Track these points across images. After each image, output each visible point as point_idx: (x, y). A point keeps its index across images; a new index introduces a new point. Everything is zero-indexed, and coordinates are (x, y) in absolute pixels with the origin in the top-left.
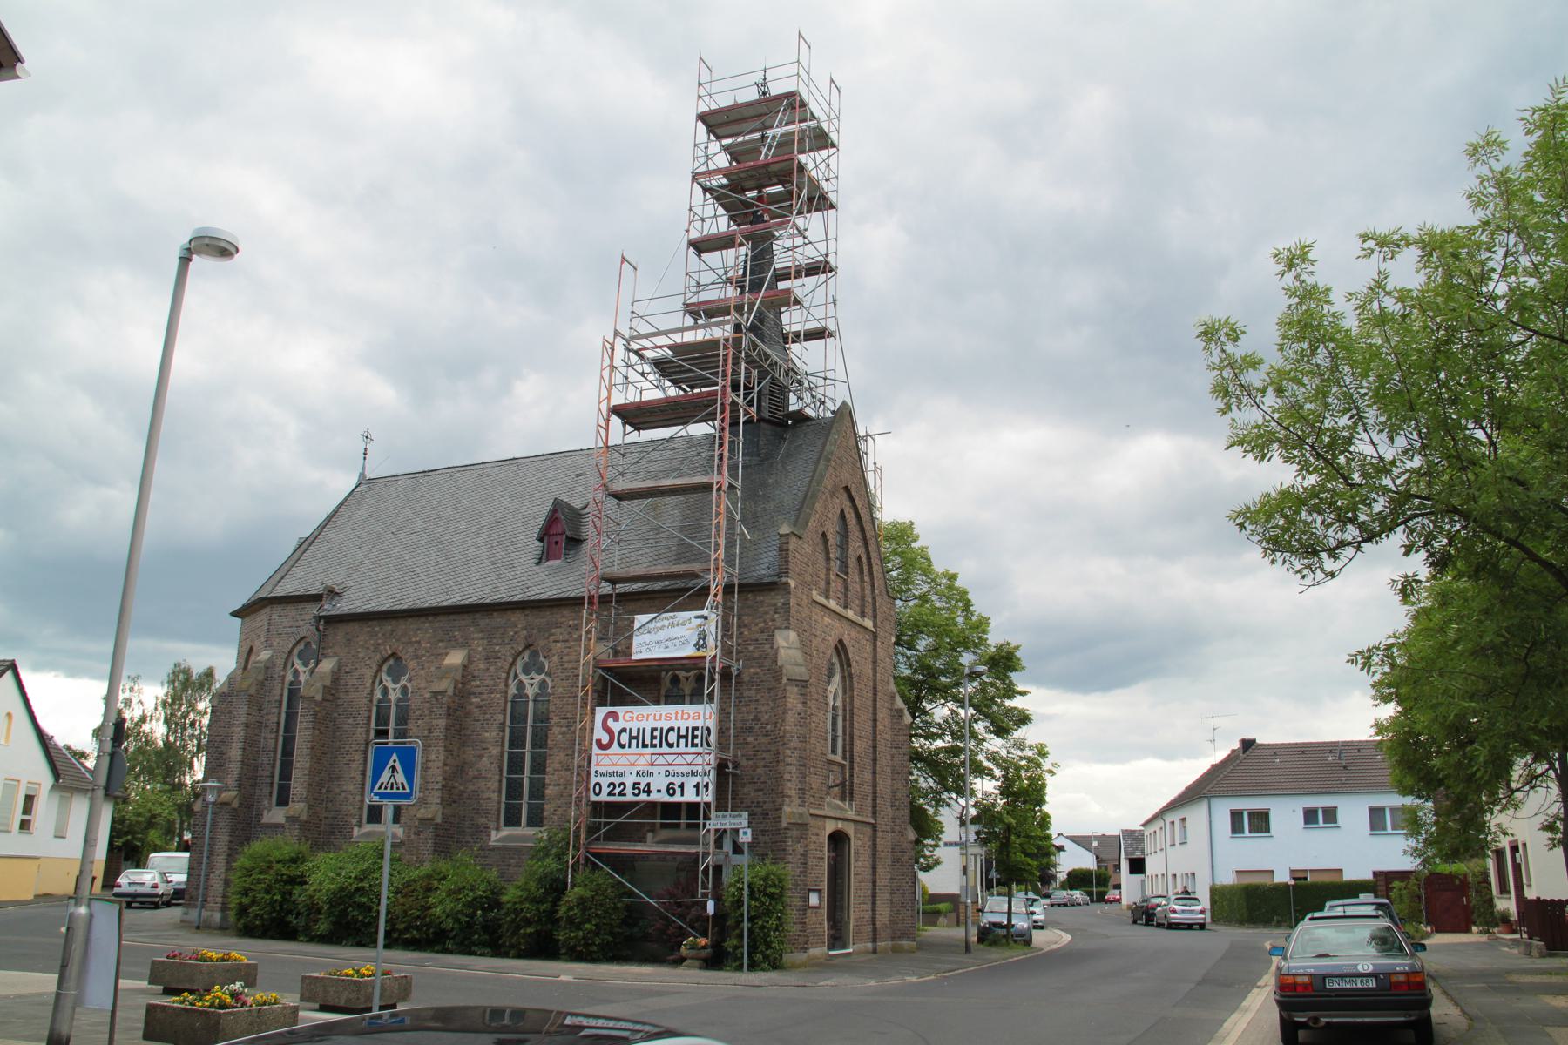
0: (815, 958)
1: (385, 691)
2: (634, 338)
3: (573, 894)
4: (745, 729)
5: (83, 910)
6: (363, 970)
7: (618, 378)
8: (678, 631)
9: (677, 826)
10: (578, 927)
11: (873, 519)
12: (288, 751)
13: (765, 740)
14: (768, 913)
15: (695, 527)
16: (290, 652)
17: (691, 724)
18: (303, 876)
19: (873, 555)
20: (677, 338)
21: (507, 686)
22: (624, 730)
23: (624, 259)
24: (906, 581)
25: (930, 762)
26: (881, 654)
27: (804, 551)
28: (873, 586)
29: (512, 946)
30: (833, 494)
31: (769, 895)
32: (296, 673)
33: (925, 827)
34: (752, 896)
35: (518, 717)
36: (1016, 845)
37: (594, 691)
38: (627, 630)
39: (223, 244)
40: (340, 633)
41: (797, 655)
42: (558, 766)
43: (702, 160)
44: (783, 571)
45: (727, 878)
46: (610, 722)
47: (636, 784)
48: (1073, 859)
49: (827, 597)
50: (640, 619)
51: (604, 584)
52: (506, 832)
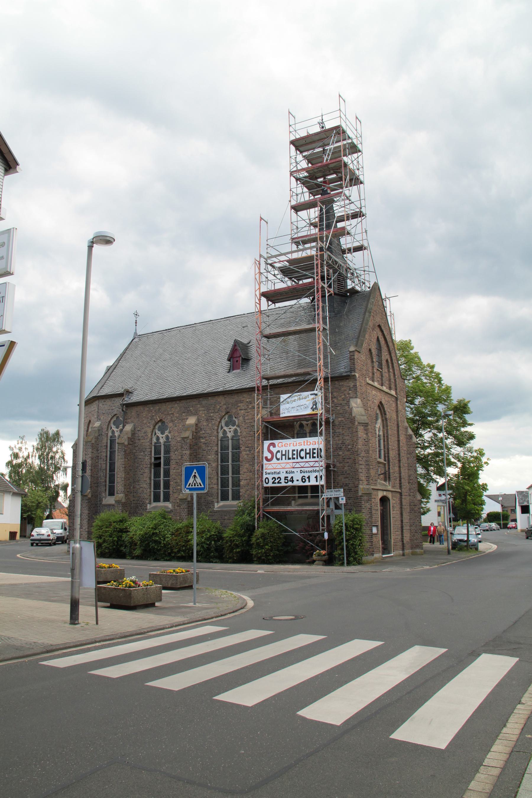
0: (376, 558)
1: (158, 439)
2: (269, 258)
3: (258, 532)
4: (338, 448)
5: (78, 545)
6: (177, 570)
7: (264, 279)
8: (303, 402)
9: (306, 497)
10: (262, 547)
11: (392, 340)
12: (112, 469)
13: (348, 453)
14: (355, 537)
15: (307, 350)
16: (110, 422)
17: (312, 447)
18: (126, 528)
19: (394, 358)
20: (290, 256)
21: (218, 432)
22: (278, 451)
23: (261, 219)
24: (410, 369)
25: (424, 461)
26: (400, 407)
27: (361, 358)
28: (394, 374)
29: (230, 558)
30: (373, 330)
31: (355, 529)
32: (113, 432)
33: (424, 493)
34: (347, 530)
35: (224, 448)
36: (465, 500)
37: (263, 433)
38: (277, 402)
39: (108, 238)
40: (133, 412)
41: (361, 410)
42: (246, 470)
43: (294, 164)
44: (352, 370)
45: (333, 522)
46: (271, 448)
47: (286, 478)
48: (491, 507)
49: (373, 381)
50: (283, 397)
51: (264, 380)
52: (222, 503)
